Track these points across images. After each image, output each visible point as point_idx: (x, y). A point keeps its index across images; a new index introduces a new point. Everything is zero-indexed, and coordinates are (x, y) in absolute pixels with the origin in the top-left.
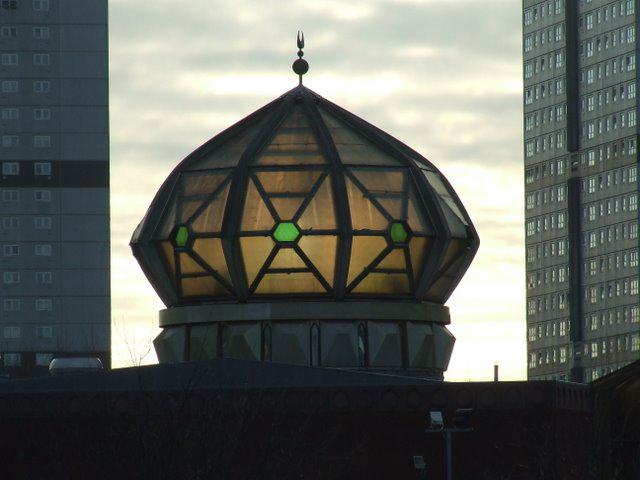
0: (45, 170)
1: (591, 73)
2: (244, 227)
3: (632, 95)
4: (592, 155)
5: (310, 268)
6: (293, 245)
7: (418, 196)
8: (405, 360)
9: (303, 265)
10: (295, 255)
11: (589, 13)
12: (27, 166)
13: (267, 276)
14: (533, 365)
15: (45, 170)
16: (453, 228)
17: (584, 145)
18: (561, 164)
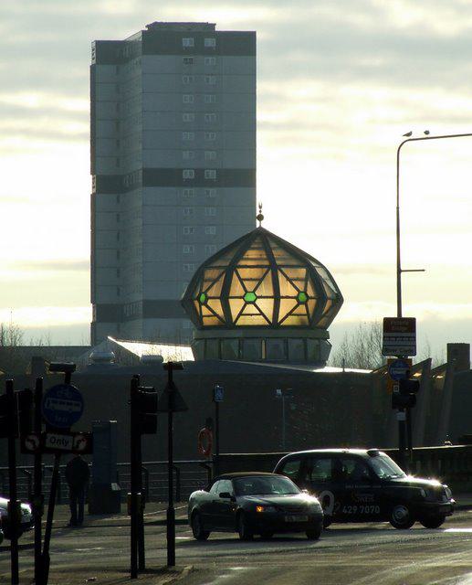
5: (262, 313)
8: (287, 354)
12: (199, 172)
15: (212, 175)
16: (329, 294)
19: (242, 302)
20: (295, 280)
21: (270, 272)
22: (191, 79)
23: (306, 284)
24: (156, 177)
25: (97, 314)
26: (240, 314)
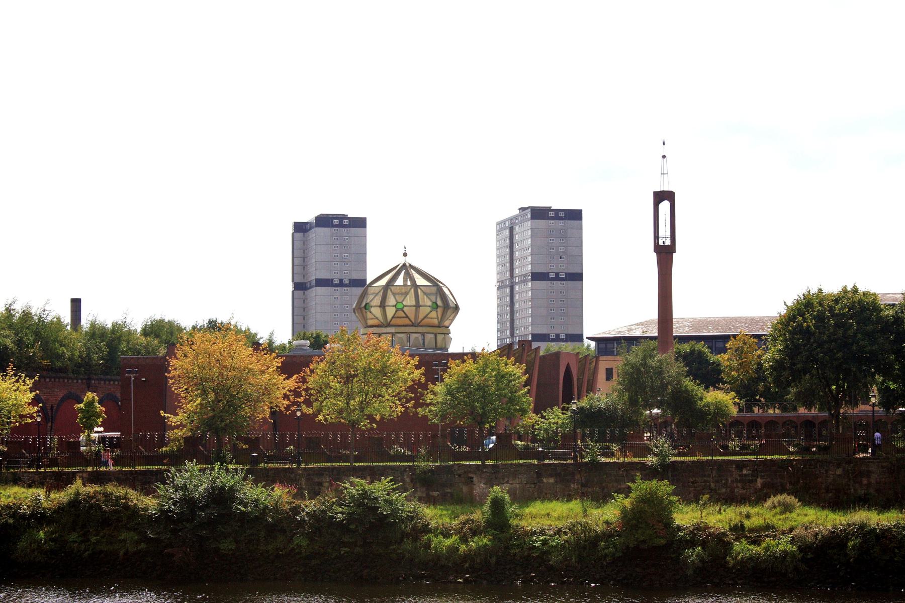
0: (347, 282)
1: (517, 253)
2: (386, 304)
3: (530, 260)
4: (517, 278)
5: (407, 317)
6: (402, 310)
7: (440, 294)
8: (424, 343)
9: (404, 315)
10: (402, 313)
11: (516, 234)
12: (341, 280)
13: (394, 319)
14: (499, 344)
15: (347, 282)
16: (451, 305)
17: (515, 276)
18: (508, 282)
19: (394, 309)
20: (403, 317)
21: (413, 290)
22: (337, 238)
23: (436, 298)
24: (321, 283)
25: (324, 218)
26: (393, 317)
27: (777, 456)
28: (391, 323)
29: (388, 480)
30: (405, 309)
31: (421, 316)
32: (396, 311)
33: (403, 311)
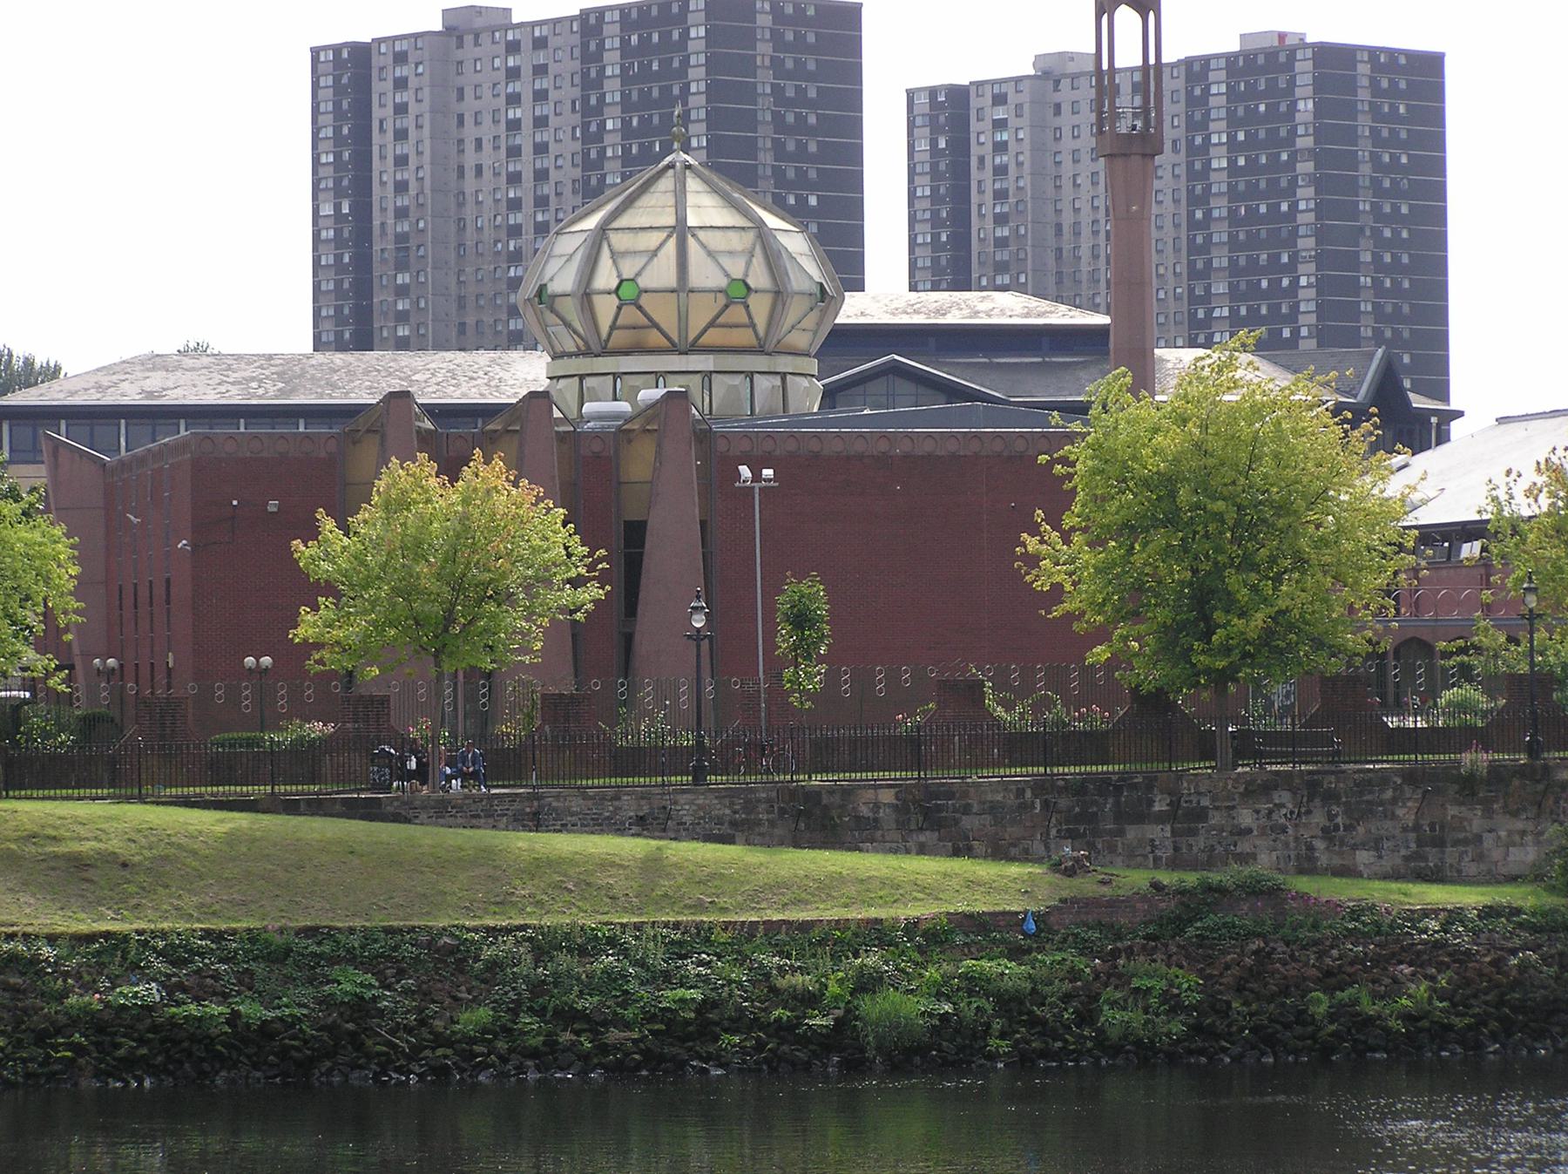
19: (613, 301)
26: (613, 327)
27: (1072, 769)
28: (610, 345)
29: (15, 928)
30: (645, 301)
31: (605, 324)
32: (619, 308)
33: (640, 308)
